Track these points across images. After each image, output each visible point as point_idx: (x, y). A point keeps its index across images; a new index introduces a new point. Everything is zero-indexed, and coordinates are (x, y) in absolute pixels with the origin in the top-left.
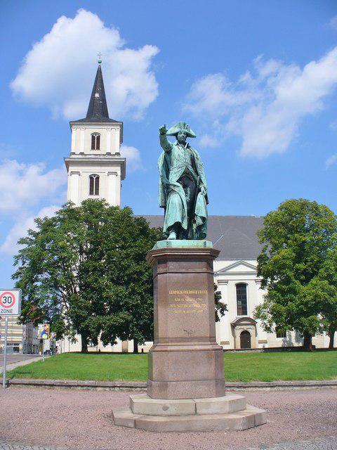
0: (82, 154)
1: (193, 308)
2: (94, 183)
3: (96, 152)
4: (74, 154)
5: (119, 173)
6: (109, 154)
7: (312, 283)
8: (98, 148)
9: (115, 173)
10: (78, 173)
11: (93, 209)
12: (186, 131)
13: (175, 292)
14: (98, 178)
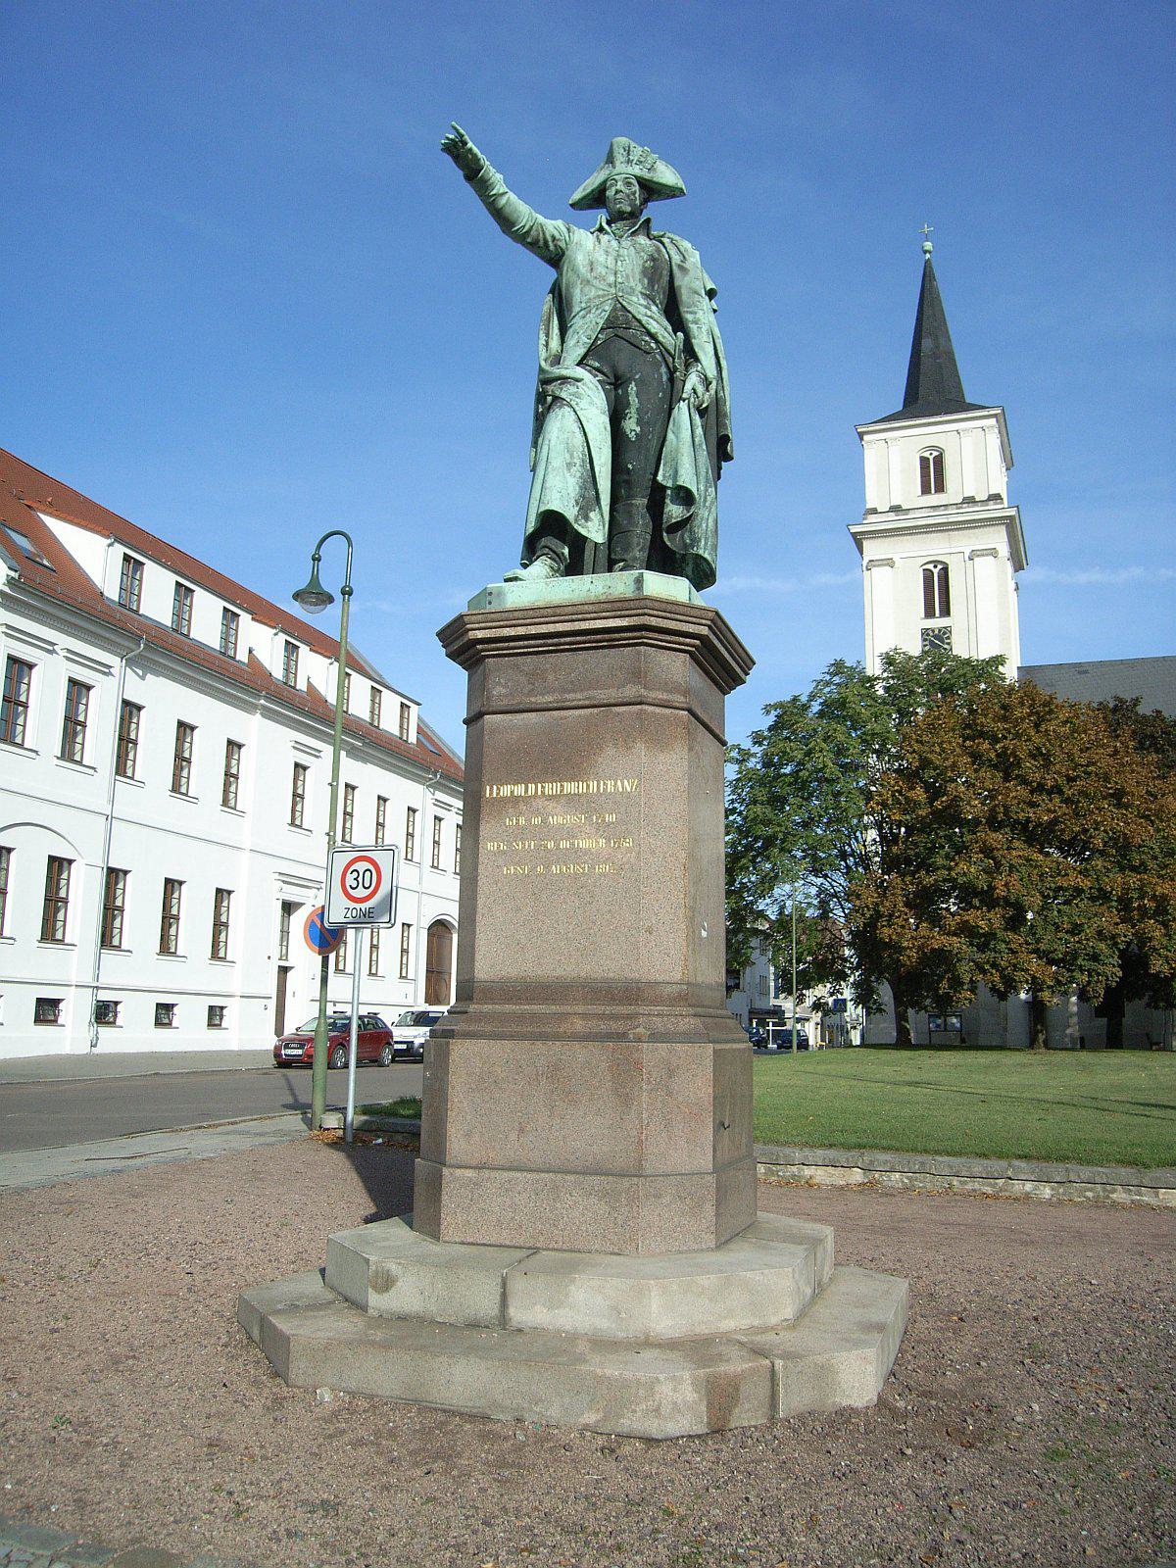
0: (896, 509)
1: (577, 854)
2: (937, 591)
3: (934, 499)
4: (874, 511)
5: (1004, 550)
6: (970, 501)
7: (639, 581)
8: (940, 488)
9: (993, 553)
10: (890, 563)
11: (937, 675)
12: (637, 170)
13: (506, 790)
14: (945, 570)
